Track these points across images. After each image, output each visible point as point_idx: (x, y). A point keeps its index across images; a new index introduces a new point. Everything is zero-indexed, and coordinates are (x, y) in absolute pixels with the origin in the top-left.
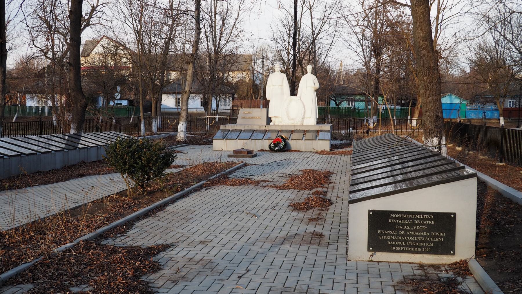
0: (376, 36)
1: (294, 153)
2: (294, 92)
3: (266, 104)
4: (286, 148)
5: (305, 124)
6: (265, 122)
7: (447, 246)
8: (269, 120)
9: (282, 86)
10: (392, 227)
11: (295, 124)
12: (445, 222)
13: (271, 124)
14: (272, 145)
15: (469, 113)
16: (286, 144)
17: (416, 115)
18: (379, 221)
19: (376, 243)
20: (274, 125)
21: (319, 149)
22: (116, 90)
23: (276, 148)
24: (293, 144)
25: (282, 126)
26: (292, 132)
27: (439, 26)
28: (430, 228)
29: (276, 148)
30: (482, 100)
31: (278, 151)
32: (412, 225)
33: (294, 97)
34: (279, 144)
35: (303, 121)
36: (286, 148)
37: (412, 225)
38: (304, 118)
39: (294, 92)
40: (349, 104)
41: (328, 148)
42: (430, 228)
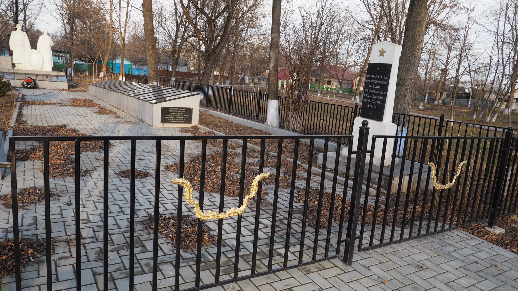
0: (69, 8)
1: (41, 90)
2: (34, 46)
3: (11, 53)
4: (35, 87)
5: (43, 70)
6: (10, 66)
7: (189, 120)
8: (14, 65)
9: (24, 41)
10: (170, 113)
11: (36, 70)
12: (189, 111)
13: (15, 68)
14: (25, 83)
15: (133, 71)
16: (35, 84)
17: (104, 69)
18: (165, 111)
19: (164, 120)
20: (18, 70)
21: (61, 88)
22: (268, 66)
23: (29, 86)
24: (40, 84)
25: (27, 70)
26: (37, 75)
27: (129, 14)
28: (184, 114)
29: (29, 86)
30: (141, 63)
31: (30, 88)
32: (177, 112)
33: (34, 50)
34: (31, 83)
35: (42, 68)
36: (35, 87)
37: (177, 112)
38: (43, 66)
39: (34, 46)
40: (59, 59)
41: (66, 88)
42: (184, 114)
